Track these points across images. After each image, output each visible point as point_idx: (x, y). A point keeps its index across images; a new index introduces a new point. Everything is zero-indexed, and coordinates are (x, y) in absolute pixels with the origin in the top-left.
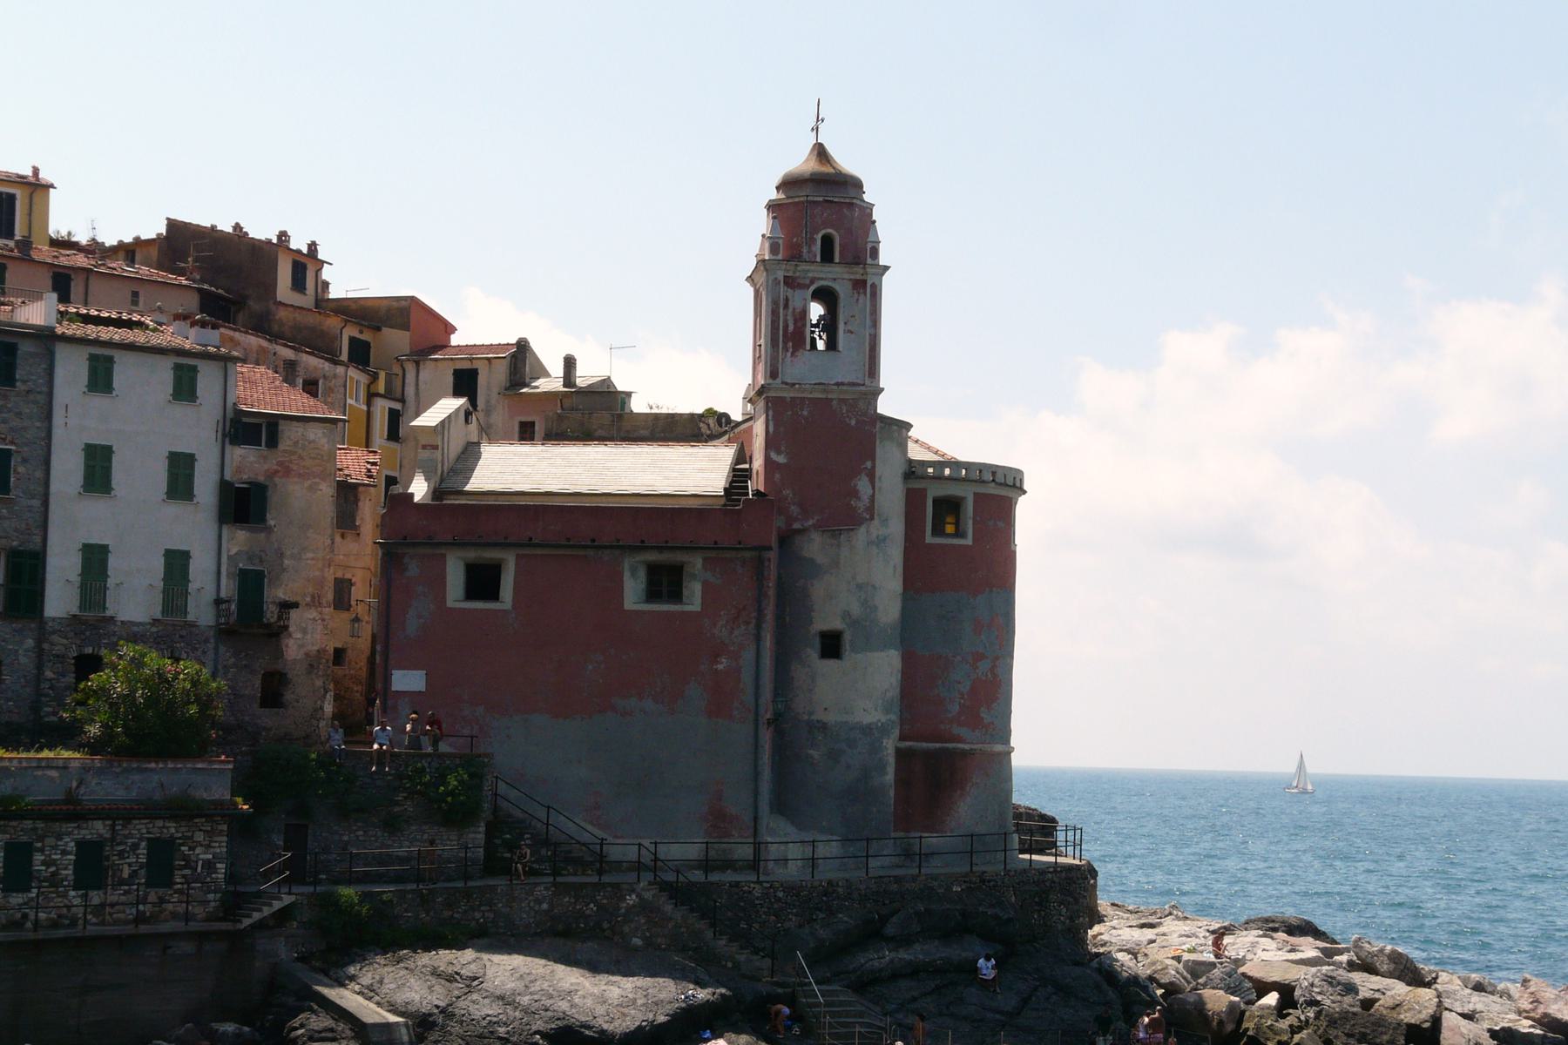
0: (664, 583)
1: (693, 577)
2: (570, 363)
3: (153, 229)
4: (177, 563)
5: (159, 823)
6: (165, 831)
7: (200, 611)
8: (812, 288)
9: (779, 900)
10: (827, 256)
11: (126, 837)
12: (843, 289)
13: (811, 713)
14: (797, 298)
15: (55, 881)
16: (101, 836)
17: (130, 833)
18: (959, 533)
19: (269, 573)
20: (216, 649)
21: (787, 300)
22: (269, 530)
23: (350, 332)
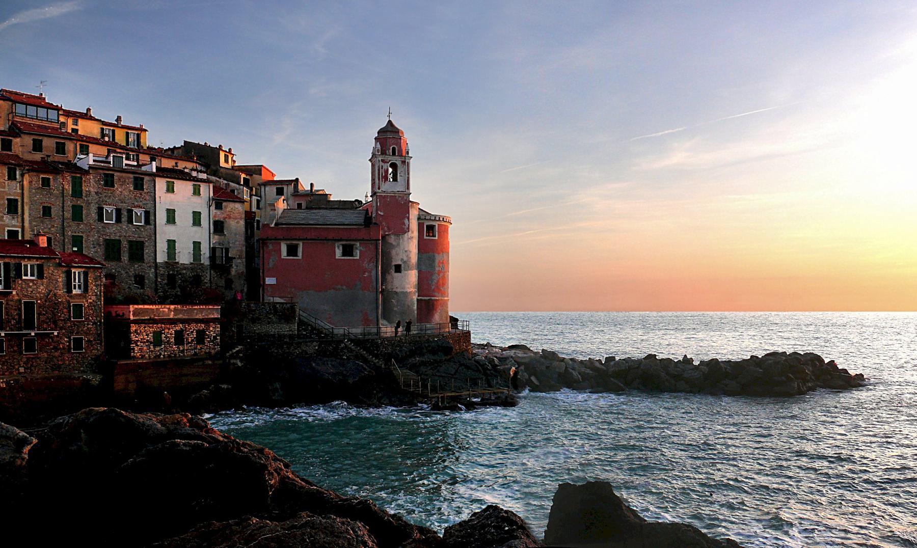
1: (357, 248)
2: (312, 185)
4: (197, 245)
8: (390, 163)
9: (386, 344)
10: (394, 154)
11: (189, 329)
12: (399, 163)
13: (392, 289)
14: (386, 166)
15: (169, 342)
16: (181, 329)
20: (210, 272)
21: (382, 166)
23: (243, 176)
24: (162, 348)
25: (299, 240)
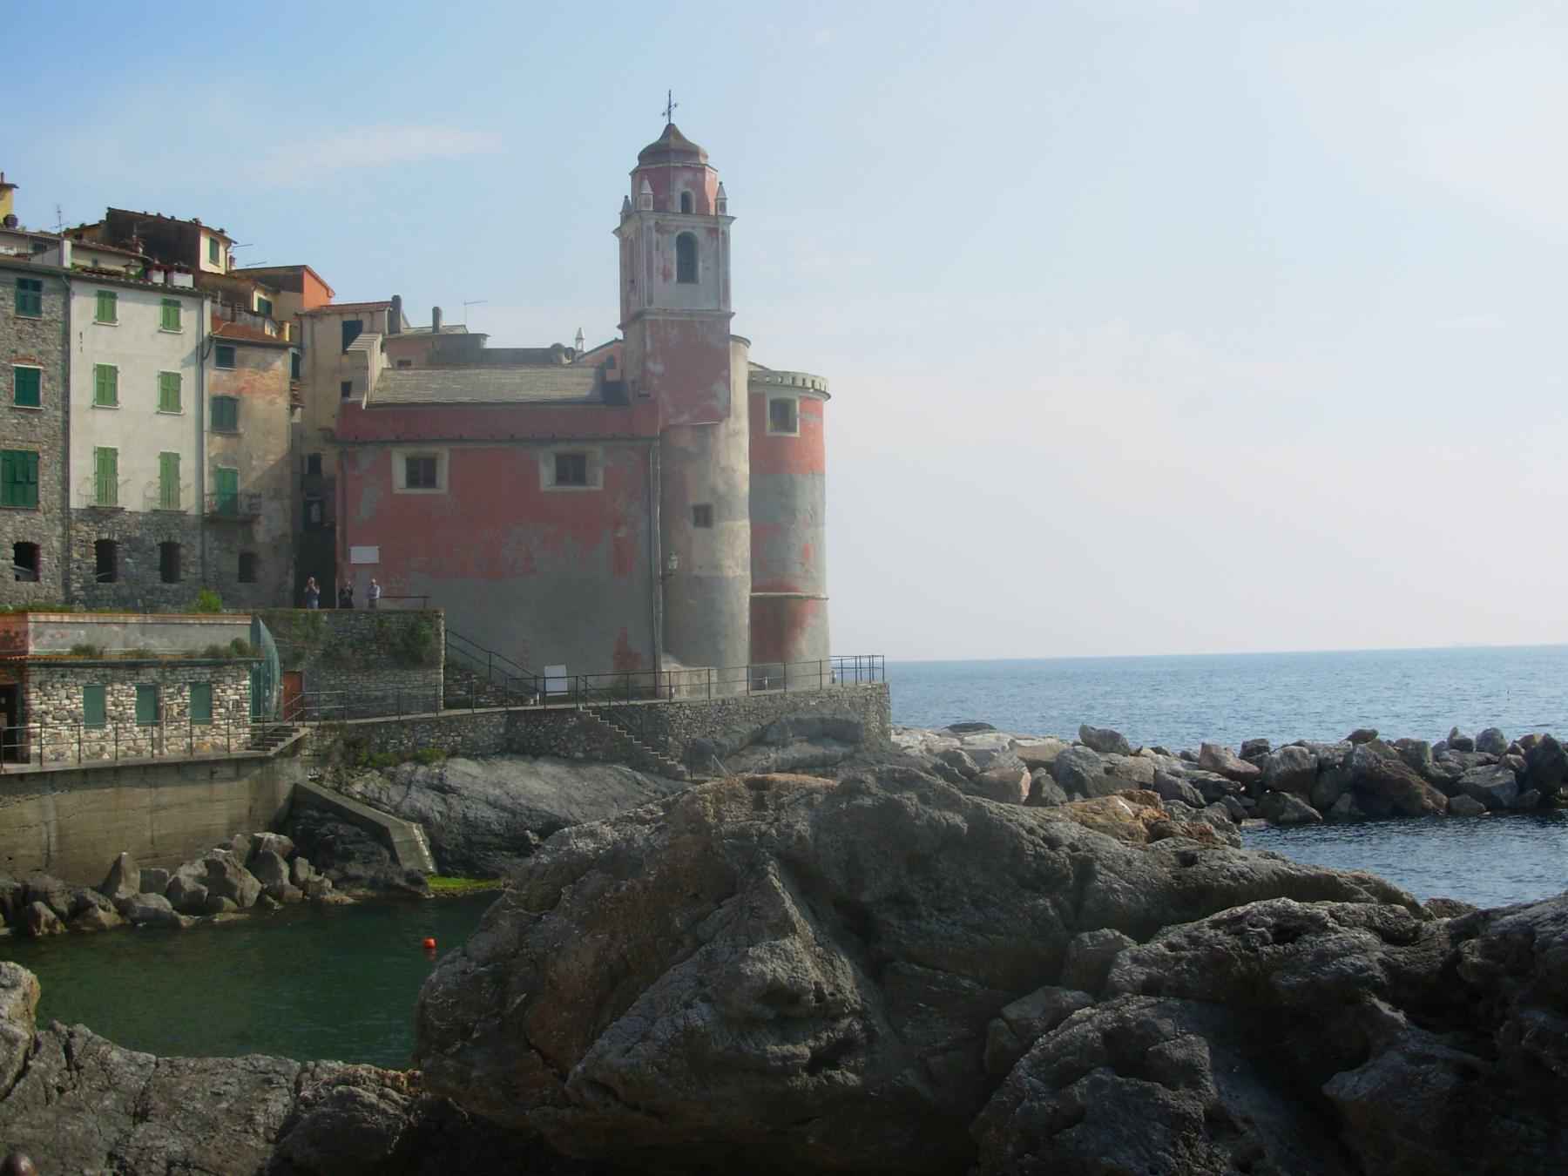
0: (571, 470)
2: (436, 313)
4: (170, 463)
6: (203, 676)
7: (188, 502)
12: (700, 235)
16: (154, 681)
17: (177, 679)
19: (241, 471)
21: (658, 243)
22: (236, 435)
24: (107, 734)
25: (440, 441)
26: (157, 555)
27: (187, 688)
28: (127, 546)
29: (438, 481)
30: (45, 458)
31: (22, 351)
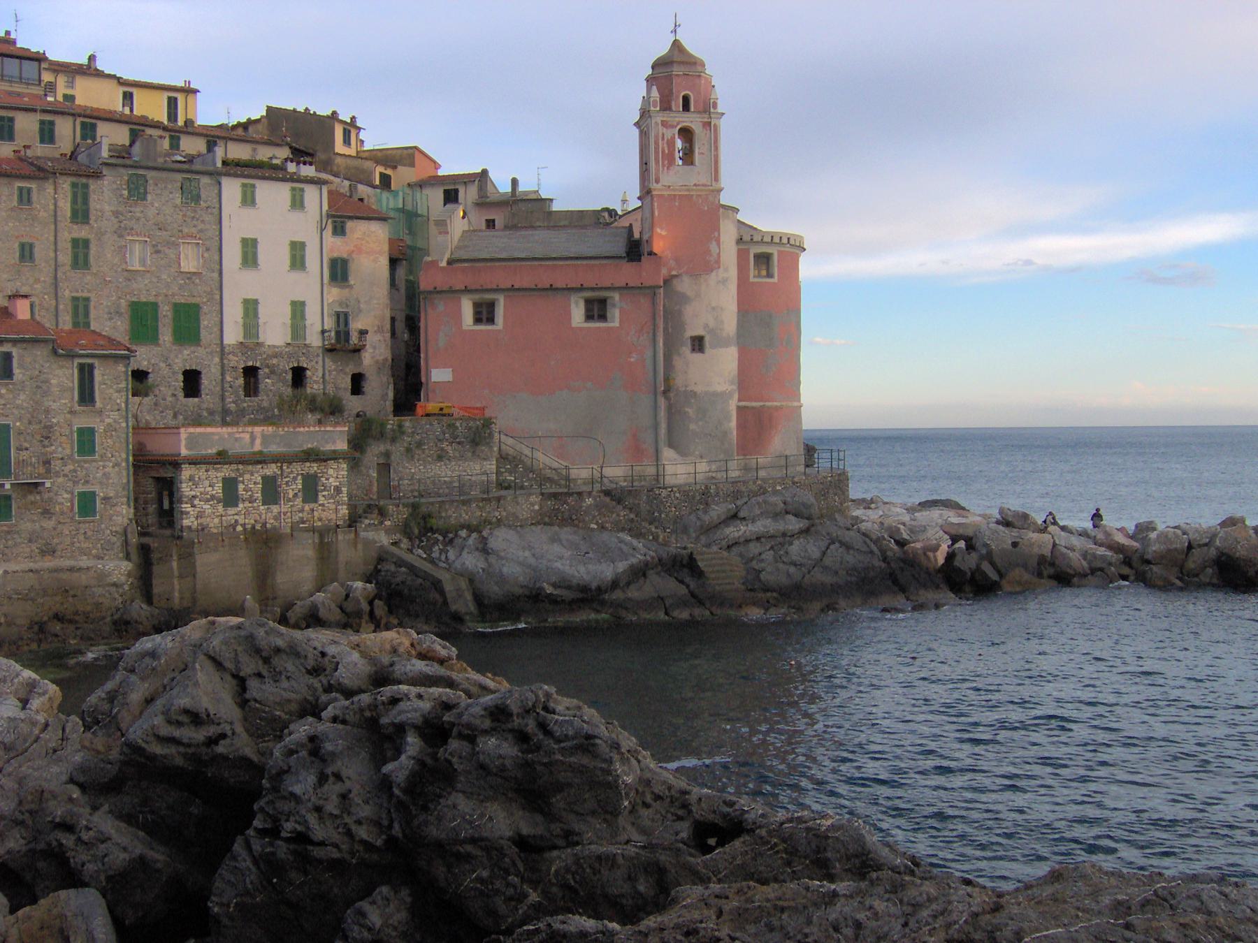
1: (614, 305)
2: (515, 182)
3: (258, 113)
4: (298, 309)
5: (308, 464)
7: (314, 339)
12: (697, 128)
18: (770, 275)
22: (350, 287)
25: (498, 290)
26: (289, 377)
27: (300, 477)
28: (267, 370)
29: (496, 320)
30: (205, 309)
31: (186, 230)
